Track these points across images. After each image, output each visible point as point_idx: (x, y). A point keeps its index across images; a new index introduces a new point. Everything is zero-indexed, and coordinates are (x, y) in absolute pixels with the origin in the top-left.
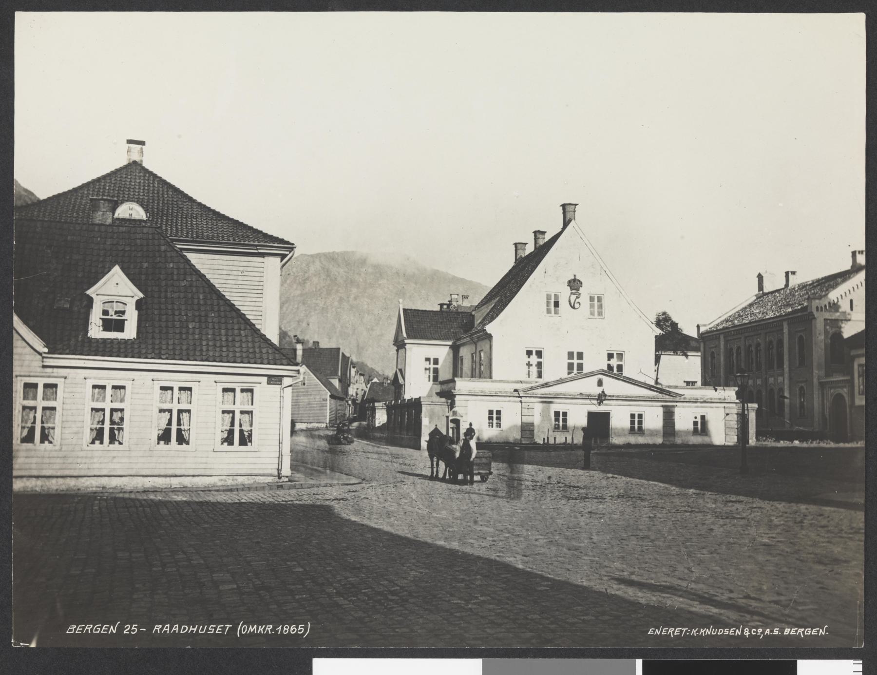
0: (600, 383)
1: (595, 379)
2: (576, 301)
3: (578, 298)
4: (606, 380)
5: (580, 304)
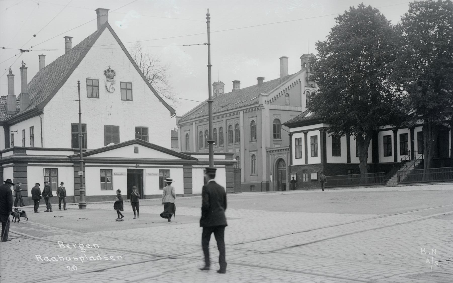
0: (136, 151)
1: (131, 148)
2: (111, 87)
3: (112, 84)
4: (141, 148)
5: (114, 89)
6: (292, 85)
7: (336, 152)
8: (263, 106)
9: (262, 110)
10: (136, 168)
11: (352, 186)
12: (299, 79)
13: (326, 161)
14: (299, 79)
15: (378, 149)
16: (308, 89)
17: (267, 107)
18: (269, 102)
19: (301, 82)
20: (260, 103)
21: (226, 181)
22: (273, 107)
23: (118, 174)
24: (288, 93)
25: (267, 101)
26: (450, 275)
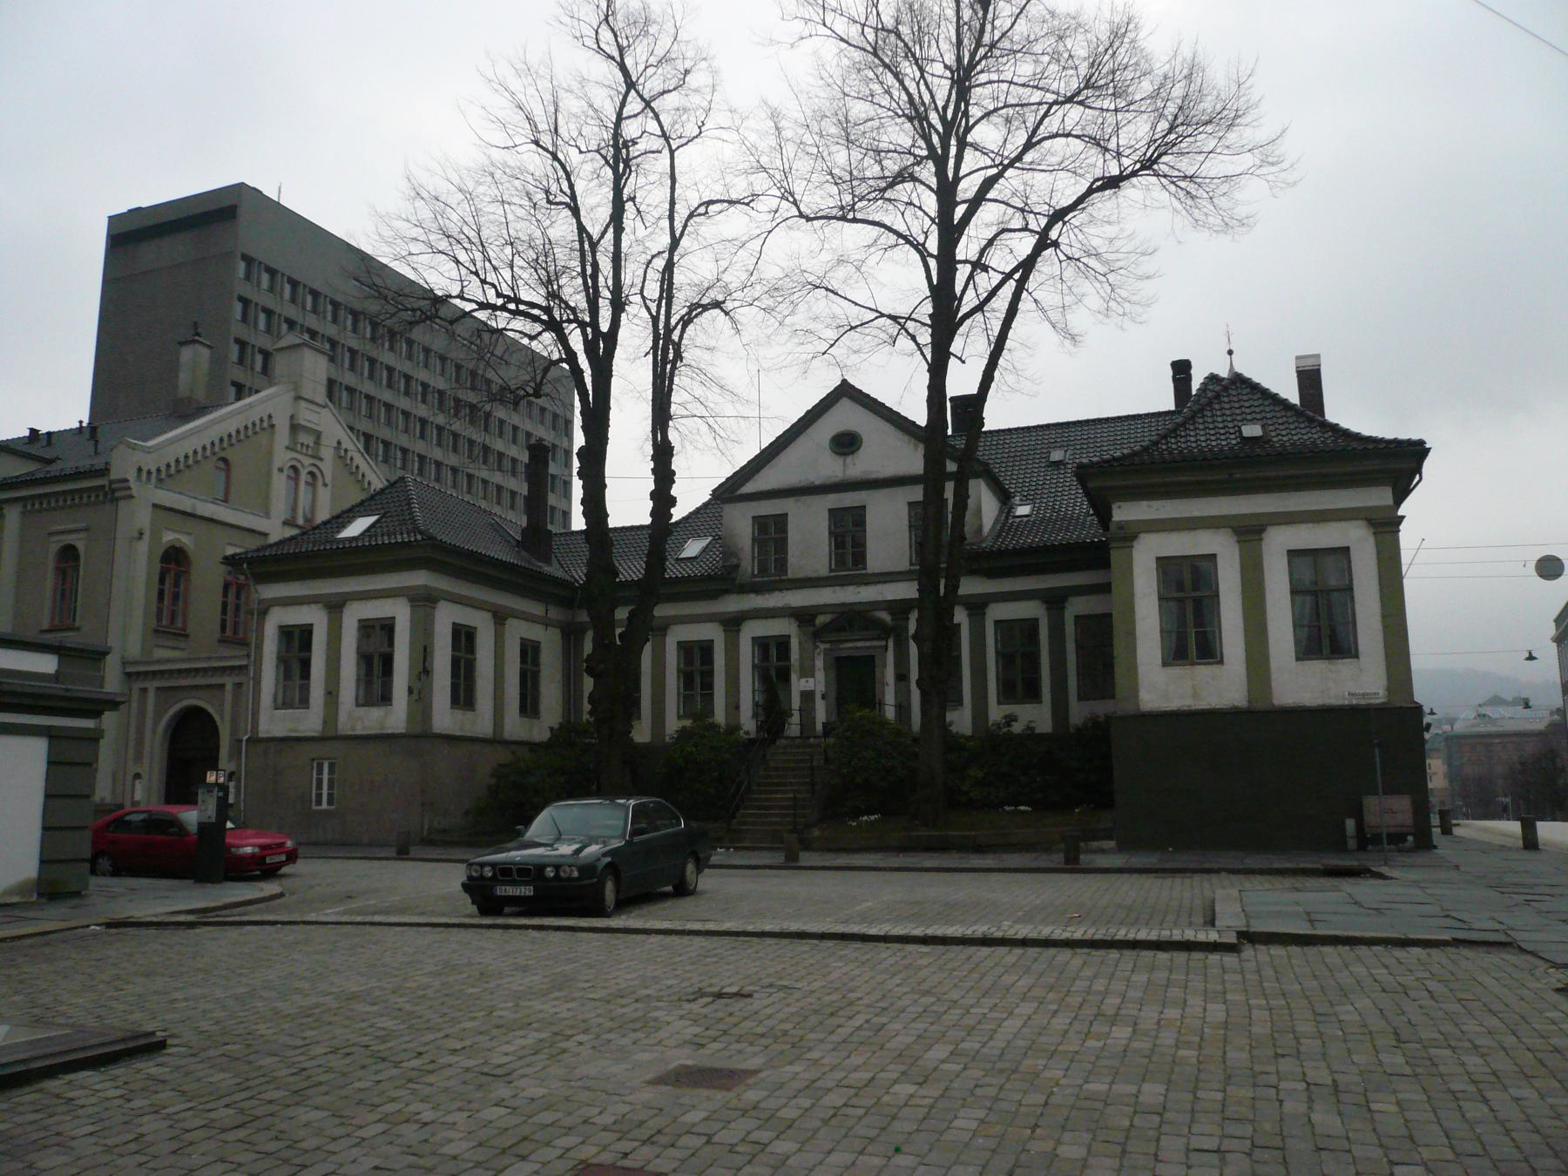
6: (182, 459)
7: (463, 696)
8: (130, 488)
9: (122, 504)
10: (928, 927)
11: (942, 847)
12: (270, 417)
13: (1113, 685)
14: (270, 417)
15: (1246, 630)
16: (299, 461)
17: (148, 495)
18: (154, 476)
19: (272, 426)
20: (114, 475)
21: (41, 853)
22: (166, 498)
23: (74, 738)
24: (229, 457)
25: (145, 469)
26: (18, 943)
